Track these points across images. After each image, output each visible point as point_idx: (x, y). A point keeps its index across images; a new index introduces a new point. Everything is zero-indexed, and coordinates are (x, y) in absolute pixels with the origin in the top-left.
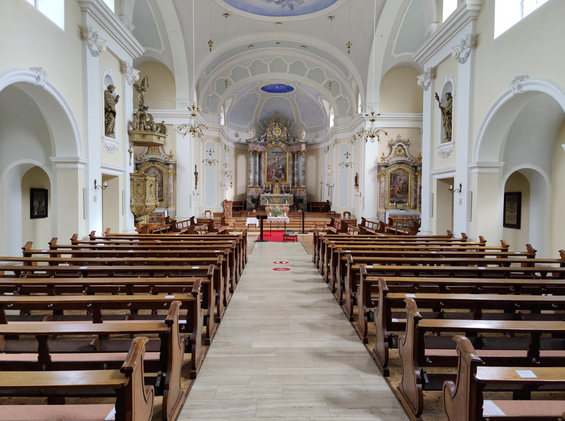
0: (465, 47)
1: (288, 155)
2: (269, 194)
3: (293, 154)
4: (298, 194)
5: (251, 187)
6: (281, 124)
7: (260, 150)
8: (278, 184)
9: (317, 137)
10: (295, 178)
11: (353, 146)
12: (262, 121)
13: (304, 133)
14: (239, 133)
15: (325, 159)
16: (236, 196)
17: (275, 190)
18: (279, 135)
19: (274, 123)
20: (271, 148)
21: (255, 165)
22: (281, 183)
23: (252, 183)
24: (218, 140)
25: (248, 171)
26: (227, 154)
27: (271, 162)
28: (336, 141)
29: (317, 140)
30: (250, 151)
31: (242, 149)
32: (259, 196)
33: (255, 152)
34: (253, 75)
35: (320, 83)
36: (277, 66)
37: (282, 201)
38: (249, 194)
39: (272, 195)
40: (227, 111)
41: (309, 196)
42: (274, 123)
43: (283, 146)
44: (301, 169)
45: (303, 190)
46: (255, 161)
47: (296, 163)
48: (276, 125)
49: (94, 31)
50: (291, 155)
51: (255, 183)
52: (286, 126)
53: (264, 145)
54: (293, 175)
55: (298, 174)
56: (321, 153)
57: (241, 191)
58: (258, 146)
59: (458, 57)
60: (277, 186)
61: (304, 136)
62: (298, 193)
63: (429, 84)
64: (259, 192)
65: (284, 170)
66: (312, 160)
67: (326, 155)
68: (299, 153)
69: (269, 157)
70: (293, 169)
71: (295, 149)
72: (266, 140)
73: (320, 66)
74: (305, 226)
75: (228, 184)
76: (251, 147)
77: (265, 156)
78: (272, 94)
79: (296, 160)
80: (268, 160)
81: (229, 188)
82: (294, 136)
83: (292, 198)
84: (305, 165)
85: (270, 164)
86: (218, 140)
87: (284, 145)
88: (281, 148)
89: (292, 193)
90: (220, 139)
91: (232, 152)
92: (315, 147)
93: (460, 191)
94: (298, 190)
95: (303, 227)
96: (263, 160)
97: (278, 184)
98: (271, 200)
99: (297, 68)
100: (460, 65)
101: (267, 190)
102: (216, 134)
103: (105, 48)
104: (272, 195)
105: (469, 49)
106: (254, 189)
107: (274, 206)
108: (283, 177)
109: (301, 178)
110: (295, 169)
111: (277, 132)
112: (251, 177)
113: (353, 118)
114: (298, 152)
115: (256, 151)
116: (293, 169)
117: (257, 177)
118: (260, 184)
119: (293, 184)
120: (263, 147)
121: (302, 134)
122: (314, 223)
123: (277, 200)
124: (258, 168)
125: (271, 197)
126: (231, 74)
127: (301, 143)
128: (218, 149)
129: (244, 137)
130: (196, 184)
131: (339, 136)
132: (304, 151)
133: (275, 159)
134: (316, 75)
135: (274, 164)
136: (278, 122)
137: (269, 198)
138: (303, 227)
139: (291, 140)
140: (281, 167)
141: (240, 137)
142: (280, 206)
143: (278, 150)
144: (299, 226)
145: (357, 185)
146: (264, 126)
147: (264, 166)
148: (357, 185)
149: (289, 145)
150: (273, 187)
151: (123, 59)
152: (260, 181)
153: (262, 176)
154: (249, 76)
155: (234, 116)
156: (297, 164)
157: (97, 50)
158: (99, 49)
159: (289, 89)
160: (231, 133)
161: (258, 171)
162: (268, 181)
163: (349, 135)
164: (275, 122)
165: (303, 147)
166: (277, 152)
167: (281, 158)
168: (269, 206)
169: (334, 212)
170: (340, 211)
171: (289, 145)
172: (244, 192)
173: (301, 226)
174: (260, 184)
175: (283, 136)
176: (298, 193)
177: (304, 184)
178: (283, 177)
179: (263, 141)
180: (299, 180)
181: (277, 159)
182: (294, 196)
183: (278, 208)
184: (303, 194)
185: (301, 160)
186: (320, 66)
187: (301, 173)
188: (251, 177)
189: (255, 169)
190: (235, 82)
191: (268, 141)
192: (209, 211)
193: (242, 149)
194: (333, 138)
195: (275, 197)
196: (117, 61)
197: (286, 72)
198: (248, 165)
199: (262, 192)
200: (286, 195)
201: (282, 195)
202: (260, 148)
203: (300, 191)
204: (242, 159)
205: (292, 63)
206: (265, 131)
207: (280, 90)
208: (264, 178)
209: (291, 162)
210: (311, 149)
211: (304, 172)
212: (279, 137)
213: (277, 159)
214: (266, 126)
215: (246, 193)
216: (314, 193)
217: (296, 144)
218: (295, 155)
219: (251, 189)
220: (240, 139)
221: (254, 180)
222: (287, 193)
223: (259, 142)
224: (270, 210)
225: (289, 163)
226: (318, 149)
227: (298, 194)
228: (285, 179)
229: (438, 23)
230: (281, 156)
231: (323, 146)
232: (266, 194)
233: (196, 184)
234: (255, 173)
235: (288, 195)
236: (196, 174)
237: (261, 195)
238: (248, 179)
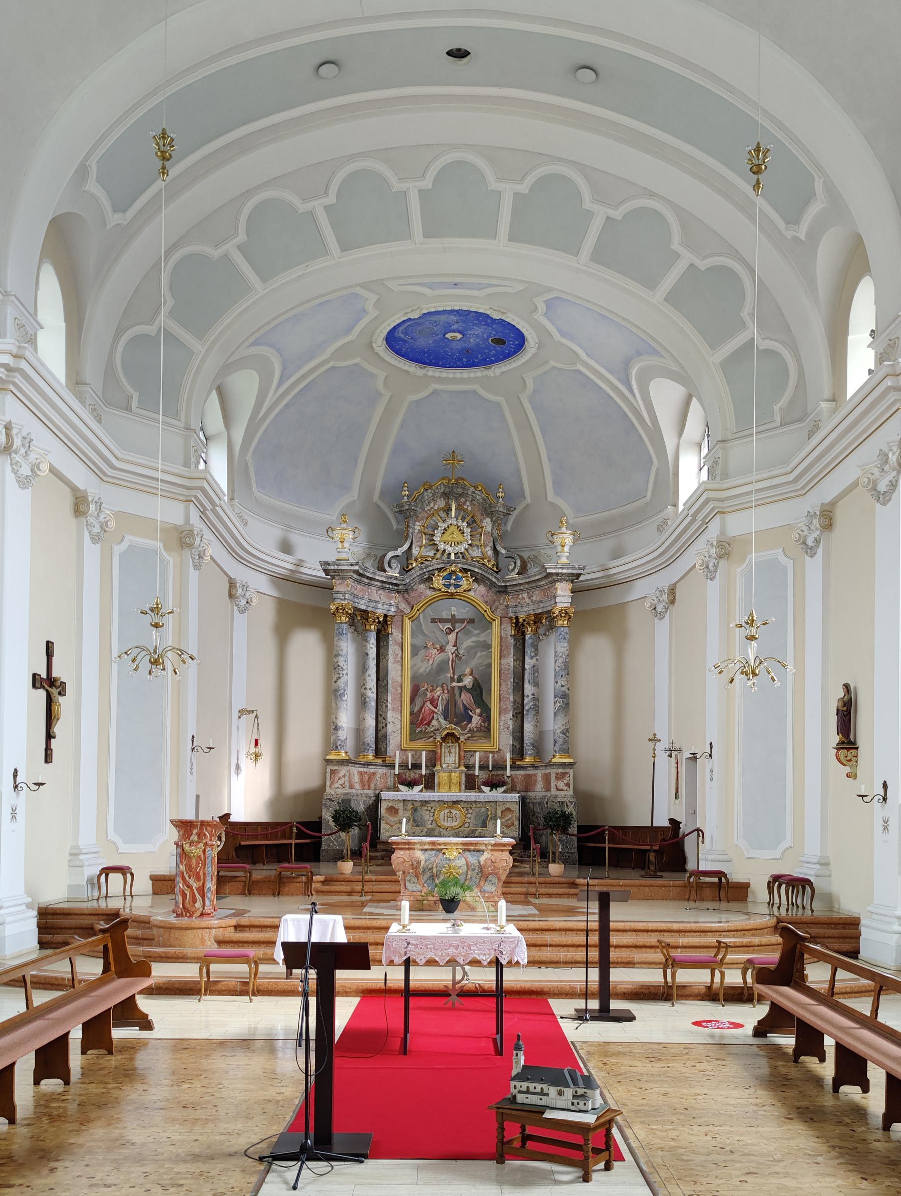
0: (887, 468)
1: (499, 633)
2: (417, 793)
3: (519, 627)
4: (538, 791)
5: (342, 762)
6: (468, 506)
7: (380, 612)
8: (455, 750)
9: (617, 554)
10: (528, 727)
11: (814, 566)
12: (391, 493)
13: (568, 539)
14: (296, 538)
15: (656, 644)
16: (278, 798)
17: (441, 776)
18: (462, 548)
19: (441, 503)
20: (431, 602)
21: (362, 669)
22: (470, 746)
23: (350, 745)
24: (183, 539)
25: (333, 694)
26: (241, 621)
27: (426, 658)
28: (725, 549)
29: (620, 568)
30: (340, 609)
31: (308, 603)
32: (378, 799)
33: (359, 619)
34: (345, 247)
35: (651, 283)
36: (455, 204)
37: (471, 820)
38: (336, 790)
39: (428, 795)
40: (239, 435)
41: (584, 798)
42: (441, 503)
43: (478, 593)
44: (550, 687)
45: (560, 777)
46: (363, 656)
47: (529, 663)
48: (448, 510)
49: (24, 434)
50: (509, 631)
51: (360, 747)
52: (491, 514)
53: (400, 589)
54: (519, 714)
55: (537, 709)
56: (636, 620)
57: (303, 775)
58: (375, 594)
59: (874, 488)
60: (450, 757)
61: (564, 552)
62: (540, 785)
63: (817, 541)
64: (378, 781)
65: (479, 691)
66: (595, 651)
67: (662, 628)
68: (544, 620)
69: (419, 642)
70: (519, 687)
71: (527, 605)
72: (405, 570)
73: (652, 195)
74: (614, 954)
75: (244, 746)
76: (346, 593)
77: (402, 638)
78: (432, 371)
79: (529, 651)
80: (415, 651)
81: (246, 764)
82: (525, 555)
83: (516, 808)
84: (568, 669)
85: (424, 668)
86: (183, 539)
87: (482, 589)
88: (470, 602)
89: (513, 789)
90: (191, 533)
91: (265, 613)
92: (612, 598)
93: (885, 799)
94: (539, 773)
95: (605, 965)
96: (393, 649)
97: (455, 750)
98: (427, 817)
99: (549, 213)
100: (878, 505)
101: (412, 775)
102: (172, 513)
103: (45, 467)
104: (428, 795)
105: (895, 473)
106: (355, 770)
107: (438, 850)
108: (476, 720)
109: (553, 724)
110: (529, 689)
111: (454, 538)
112: (346, 719)
113: (811, 435)
114: (537, 619)
115: (365, 614)
116: (519, 687)
117: (370, 722)
118: (379, 752)
119: (519, 752)
120: (395, 598)
121: (557, 540)
122: (653, 939)
123: (450, 817)
124: (371, 682)
125: (425, 803)
126: (242, 237)
127: (552, 578)
128: (190, 596)
129: (313, 556)
130: (49, 736)
131: (738, 524)
132: (565, 613)
133: (442, 649)
134: (631, 247)
135: (441, 668)
136: (458, 497)
137: (415, 807)
138: (605, 965)
139: (508, 570)
140: (468, 681)
141: (300, 554)
142: (467, 848)
143: (457, 609)
144: (580, 955)
145: (848, 741)
146: (399, 513)
147: (400, 673)
148: (848, 741)
149: (504, 591)
150: (433, 761)
151: (80, 485)
152: (380, 738)
153: (391, 716)
154: (326, 252)
155: (273, 460)
156: (536, 669)
157: (30, 474)
158: (32, 470)
159: (505, 342)
160: (262, 537)
161: (372, 695)
162: (413, 737)
163: (796, 512)
164: (446, 495)
165: (563, 594)
166: (453, 620)
167: (468, 643)
168: (409, 846)
169: (720, 874)
170: (751, 867)
171: (504, 591)
172: (314, 782)
173: (594, 954)
174: (379, 752)
175: (476, 553)
176: (540, 785)
177: (566, 751)
178: (476, 720)
179: (394, 572)
180: (540, 735)
181: (450, 648)
182: (524, 802)
183: (454, 855)
184: (561, 793)
185: (552, 651)
186: (652, 195)
187: (550, 705)
188: (346, 719)
189: (361, 685)
190: (264, 279)
191: (415, 573)
192: (122, 870)
193: (308, 603)
194: (713, 531)
195: (442, 803)
196: (68, 489)
197: (494, 236)
198: (332, 668)
199: (391, 781)
200: (487, 794)
201: (472, 795)
202: (383, 604)
203: (547, 779)
204: (307, 646)
205: (524, 188)
206: (403, 535)
207: (467, 351)
208: (397, 724)
209: (510, 661)
210: (596, 604)
211: (566, 701)
212: (460, 555)
213: (450, 648)
214: (405, 514)
215: (323, 788)
216: (604, 789)
217: (533, 585)
218: (526, 631)
219: (343, 770)
220: (300, 563)
221: (359, 732)
222: (494, 785)
223: (381, 576)
224: (415, 865)
225: (501, 664)
226: (622, 606)
227: (538, 791)
228: (486, 730)
229: (834, 400)
230: (468, 634)
231: (646, 590)
232: (405, 793)
233: (49, 736)
234: (362, 702)
235: (497, 794)
236: (49, 684)
237: (385, 795)
238: (331, 727)
